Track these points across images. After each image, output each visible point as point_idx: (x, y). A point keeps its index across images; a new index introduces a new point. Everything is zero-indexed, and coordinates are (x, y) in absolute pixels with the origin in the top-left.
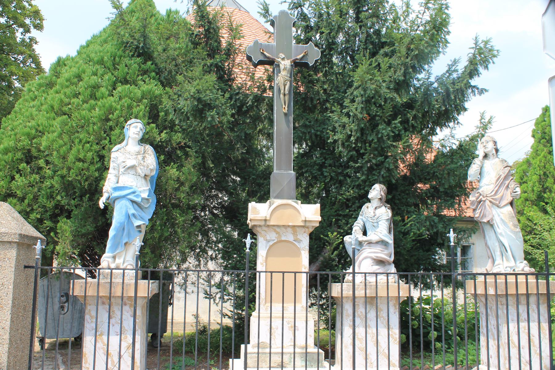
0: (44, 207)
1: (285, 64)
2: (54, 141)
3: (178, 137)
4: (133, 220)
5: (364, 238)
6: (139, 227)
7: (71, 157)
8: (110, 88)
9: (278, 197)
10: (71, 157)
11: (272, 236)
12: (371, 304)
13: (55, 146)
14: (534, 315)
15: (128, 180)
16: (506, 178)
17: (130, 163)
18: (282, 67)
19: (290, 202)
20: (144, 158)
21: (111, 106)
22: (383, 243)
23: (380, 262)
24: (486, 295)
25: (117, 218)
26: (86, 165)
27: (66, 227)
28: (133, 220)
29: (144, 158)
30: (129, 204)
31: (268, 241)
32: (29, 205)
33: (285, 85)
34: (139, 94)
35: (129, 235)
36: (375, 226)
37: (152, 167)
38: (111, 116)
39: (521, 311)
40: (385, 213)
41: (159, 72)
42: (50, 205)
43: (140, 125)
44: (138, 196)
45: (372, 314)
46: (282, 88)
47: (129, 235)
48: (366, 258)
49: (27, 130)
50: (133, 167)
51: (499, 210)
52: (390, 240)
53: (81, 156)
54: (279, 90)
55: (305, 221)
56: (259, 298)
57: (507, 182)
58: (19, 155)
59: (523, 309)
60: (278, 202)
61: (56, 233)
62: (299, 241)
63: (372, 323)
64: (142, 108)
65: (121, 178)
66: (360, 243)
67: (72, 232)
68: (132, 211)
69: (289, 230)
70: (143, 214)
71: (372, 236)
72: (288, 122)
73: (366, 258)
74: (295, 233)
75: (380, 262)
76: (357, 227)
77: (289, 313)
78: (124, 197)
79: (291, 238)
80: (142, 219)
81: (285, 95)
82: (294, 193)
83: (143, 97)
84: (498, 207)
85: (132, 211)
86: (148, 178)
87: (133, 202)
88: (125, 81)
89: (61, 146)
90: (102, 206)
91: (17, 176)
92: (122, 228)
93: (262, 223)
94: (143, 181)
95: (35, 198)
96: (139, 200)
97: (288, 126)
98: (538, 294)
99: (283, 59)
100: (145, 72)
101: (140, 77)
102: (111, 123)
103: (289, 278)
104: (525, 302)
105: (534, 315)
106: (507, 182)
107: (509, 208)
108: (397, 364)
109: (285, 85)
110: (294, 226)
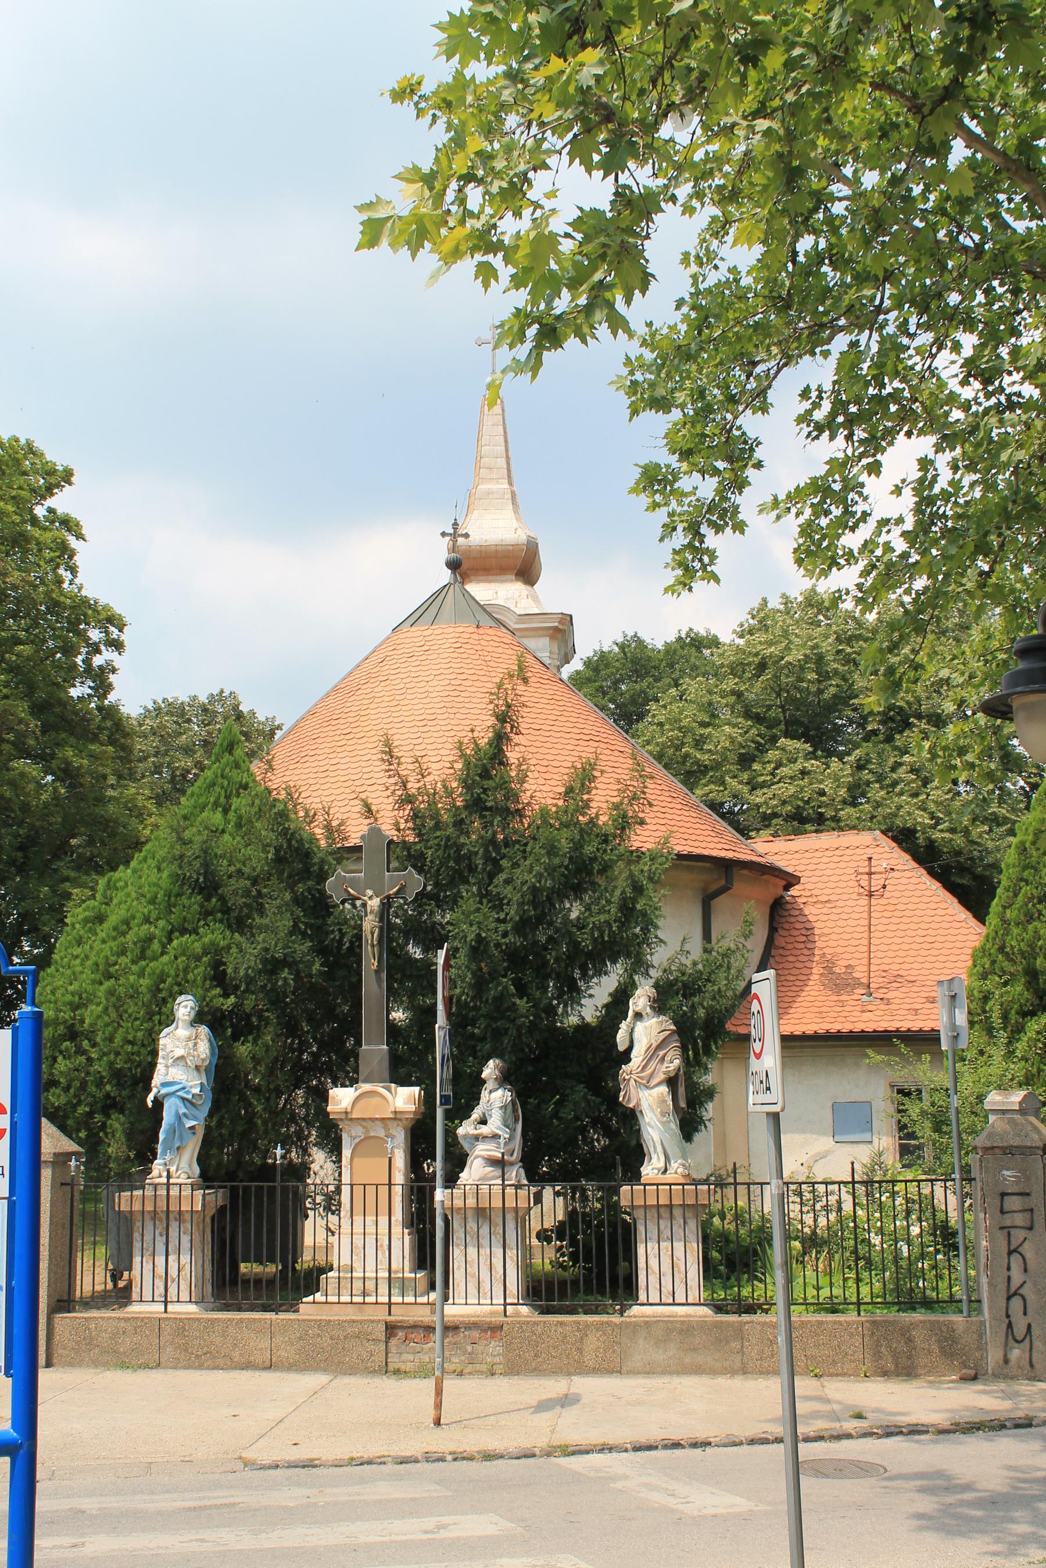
0: (93, 1096)
2: (99, 1017)
3: (249, 1002)
4: (185, 1120)
6: (192, 1128)
7: (118, 1040)
8: (164, 940)
10: (118, 1040)
11: (358, 1131)
12: (485, 1217)
14: (678, 1232)
15: (177, 1074)
16: (659, 1047)
20: (195, 1044)
21: (162, 971)
26: (136, 1048)
27: (117, 1125)
28: (185, 1120)
29: (195, 1044)
32: (75, 1096)
33: (372, 934)
34: (198, 947)
35: (181, 1138)
37: (203, 1056)
38: (162, 986)
39: (662, 1227)
41: (226, 910)
42: (100, 1095)
43: (191, 1004)
44: (188, 1092)
45: (485, 1230)
47: (181, 1138)
49: (68, 998)
50: (182, 1058)
51: (647, 1092)
53: (130, 1037)
55: (396, 1112)
57: (661, 1053)
58: (61, 1029)
59: (664, 1224)
60: (365, 1087)
61: (106, 1134)
63: (485, 1242)
64: (200, 971)
66: (477, 1138)
67: (124, 1131)
68: (183, 1110)
69: (378, 1123)
70: (196, 1112)
72: (379, 980)
73: (477, 1157)
74: (386, 1128)
76: (476, 1115)
78: (173, 1093)
79: (381, 1133)
80: (195, 1118)
81: (373, 946)
82: (386, 1074)
84: (647, 1088)
85: (183, 1110)
86: (202, 1069)
87: (183, 1099)
88: (183, 931)
89: (107, 1025)
90: (150, 1104)
91: (60, 1059)
92: (172, 1131)
93: (343, 1116)
94: (195, 1073)
95: (84, 1084)
96: (190, 1097)
97: (380, 986)
98: (645, 1206)
99: (370, 898)
100: (206, 914)
101: (202, 923)
102: (163, 994)
103: (371, 1191)
104: (668, 1215)
105: (678, 1232)
106: (661, 1053)
107: (664, 1089)
109: (372, 934)
110: (382, 1119)
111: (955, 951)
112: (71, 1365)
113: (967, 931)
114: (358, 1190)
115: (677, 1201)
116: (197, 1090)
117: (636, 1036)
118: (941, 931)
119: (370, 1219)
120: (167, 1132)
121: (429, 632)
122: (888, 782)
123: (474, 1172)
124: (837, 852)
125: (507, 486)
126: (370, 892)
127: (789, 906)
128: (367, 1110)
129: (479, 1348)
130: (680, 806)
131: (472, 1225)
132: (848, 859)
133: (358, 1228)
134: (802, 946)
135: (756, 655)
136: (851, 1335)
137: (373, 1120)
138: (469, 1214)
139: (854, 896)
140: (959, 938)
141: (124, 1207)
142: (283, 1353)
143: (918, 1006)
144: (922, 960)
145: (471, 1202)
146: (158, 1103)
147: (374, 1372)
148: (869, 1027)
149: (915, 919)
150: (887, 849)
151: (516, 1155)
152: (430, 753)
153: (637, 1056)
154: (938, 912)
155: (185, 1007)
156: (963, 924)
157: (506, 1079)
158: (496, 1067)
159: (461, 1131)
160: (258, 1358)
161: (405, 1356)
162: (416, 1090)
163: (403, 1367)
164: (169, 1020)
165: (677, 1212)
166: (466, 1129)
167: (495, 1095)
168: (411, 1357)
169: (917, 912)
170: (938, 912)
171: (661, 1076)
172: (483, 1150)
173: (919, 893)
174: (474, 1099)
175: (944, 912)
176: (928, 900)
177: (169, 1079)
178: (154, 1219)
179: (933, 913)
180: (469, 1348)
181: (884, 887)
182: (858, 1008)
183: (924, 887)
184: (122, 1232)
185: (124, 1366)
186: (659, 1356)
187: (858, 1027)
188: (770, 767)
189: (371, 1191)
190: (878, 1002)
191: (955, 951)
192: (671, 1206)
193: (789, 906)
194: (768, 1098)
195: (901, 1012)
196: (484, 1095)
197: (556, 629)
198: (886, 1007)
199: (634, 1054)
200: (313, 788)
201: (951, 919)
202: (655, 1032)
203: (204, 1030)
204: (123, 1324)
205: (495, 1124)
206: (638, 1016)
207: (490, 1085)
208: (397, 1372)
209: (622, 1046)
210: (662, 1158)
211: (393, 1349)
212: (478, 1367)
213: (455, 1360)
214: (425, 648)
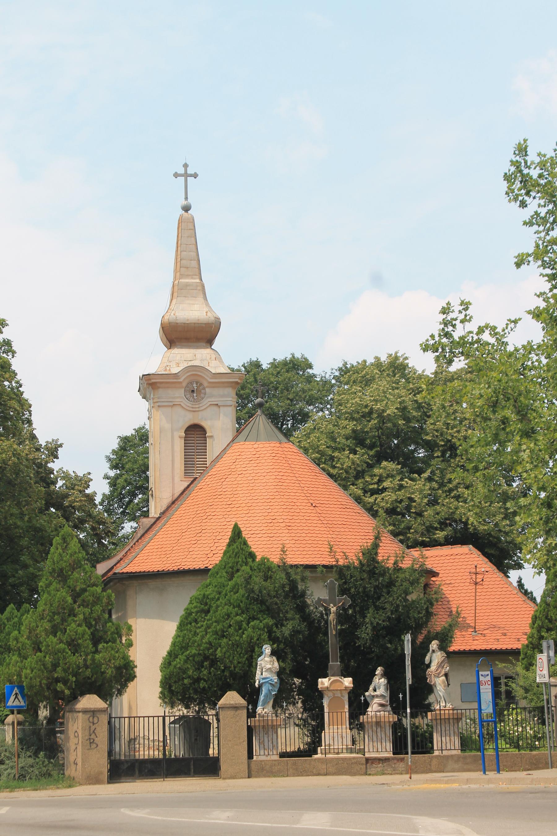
1: (333, 609)
5: (376, 693)
9: (333, 675)
11: (330, 694)
13: (226, 656)
16: (442, 662)
17: (269, 666)
18: (332, 611)
19: (338, 678)
22: (382, 696)
23: (382, 705)
24: (441, 719)
25: (264, 691)
30: (269, 685)
31: (329, 697)
36: (379, 688)
40: (383, 681)
44: (273, 681)
45: (379, 730)
46: (332, 622)
48: (375, 703)
50: (270, 669)
52: (387, 695)
54: (330, 621)
55: (346, 687)
56: (173, 461)
59: (447, 725)
60: (333, 678)
62: (343, 697)
64: (265, 636)
65: (264, 673)
66: (373, 696)
68: (271, 688)
71: (378, 693)
72: (336, 638)
73: (375, 703)
75: (382, 705)
76: (371, 688)
77: (340, 731)
79: (339, 695)
80: (275, 691)
82: (340, 674)
83: (264, 627)
85: (271, 688)
87: (271, 684)
98: (445, 719)
99: (332, 607)
103: (151, 719)
107: (444, 678)
108: (325, 714)
110: (340, 690)
111: (513, 609)
112: (256, 777)
113: (517, 599)
114: (331, 714)
115: (451, 717)
116: (276, 681)
117: (433, 658)
118: (505, 599)
119: (335, 727)
120: (264, 696)
121: (256, 446)
122: (446, 488)
124: (452, 557)
125: (198, 281)
126: (332, 605)
127: (431, 586)
128: (336, 687)
129: (397, 765)
130: (390, 542)
131: (374, 728)
132: (458, 561)
133: (331, 731)
134: (440, 607)
135: (366, 406)
136: (517, 758)
137: (337, 690)
138: (373, 724)
139: (468, 584)
140: (515, 602)
142: (330, 770)
144: (498, 614)
145: (374, 720)
146: (260, 686)
147: (362, 775)
148: (478, 648)
149: (493, 593)
150: (476, 555)
153: (433, 667)
154: (504, 589)
155: (267, 649)
156: (516, 596)
157: (385, 675)
158: (382, 670)
160: (322, 772)
161: (372, 769)
163: (371, 773)
165: (451, 721)
166: (370, 692)
167: (381, 681)
168: (374, 769)
169: (494, 589)
170: (504, 589)
171: (443, 673)
173: (494, 579)
175: (506, 589)
176: (498, 583)
177: (264, 676)
178: (272, 728)
179: (501, 590)
180: (393, 766)
181: (483, 580)
182: (471, 638)
183: (496, 576)
185: (275, 776)
186: (456, 766)
187: (473, 648)
188: (376, 479)
189: (151, 719)
190: (480, 635)
191: (513, 609)
192: (449, 719)
193: (431, 586)
194: (544, 679)
195: (491, 640)
198: (484, 638)
199: (433, 664)
200: (221, 534)
201: (510, 593)
202: (440, 657)
203: (274, 658)
204: (274, 762)
205: (381, 691)
206: (433, 651)
208: (370, 775)
209: (427, 662)
210: (444, 702)
211: (368, 767)
212: (396, 772)
213: (389, 770)
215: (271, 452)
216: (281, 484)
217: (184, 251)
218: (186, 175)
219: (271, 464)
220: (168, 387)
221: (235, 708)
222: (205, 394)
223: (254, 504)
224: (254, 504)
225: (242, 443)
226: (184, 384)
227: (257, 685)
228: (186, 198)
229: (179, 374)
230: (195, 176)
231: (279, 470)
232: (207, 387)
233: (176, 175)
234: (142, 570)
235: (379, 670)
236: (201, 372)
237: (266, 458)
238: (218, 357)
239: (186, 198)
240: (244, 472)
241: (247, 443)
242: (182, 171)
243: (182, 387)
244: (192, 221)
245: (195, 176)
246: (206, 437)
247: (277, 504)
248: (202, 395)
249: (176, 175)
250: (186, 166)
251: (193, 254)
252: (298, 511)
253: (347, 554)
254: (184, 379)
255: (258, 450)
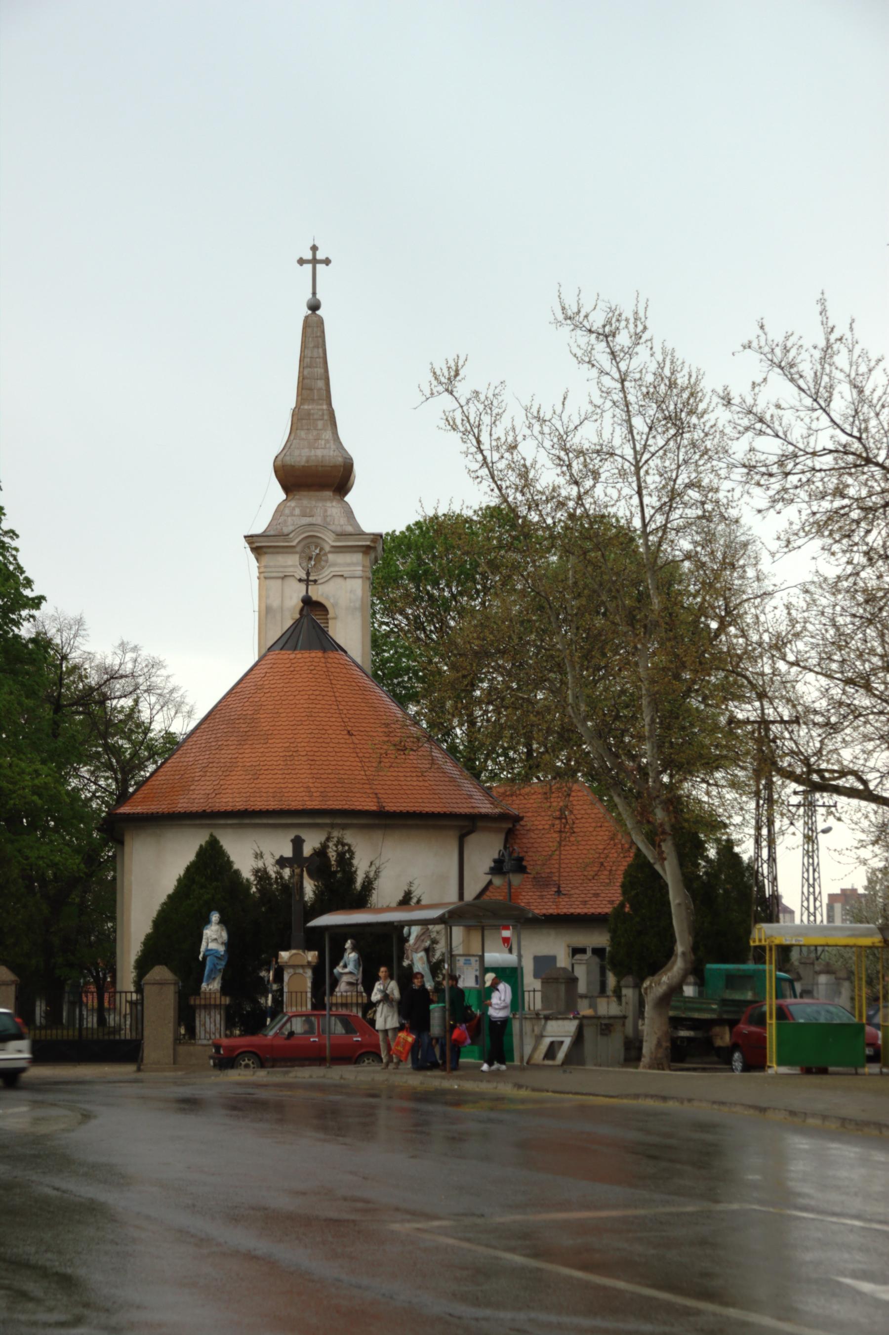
9: (295, 948)
15: (212, 946)
19: (300, 952)
60: (294, 951)
76: (341, 964)
92: (211, 971)
103: (299, 994)
123: (342, 987)
141: (192, 1002)
143: (587, 899)
151: (360, 981)
152: (300, 749)
153: (412, 940)
155: (215, 917)
157: (354, 949)
159: (335, 971)
162: (316, 953)
164: (207, 922)
166: (339, 969)
171: (422, 948)
172: (345, 979)
174: (341, 957)
184: (140, 1030)
189: (299, 994)
196: (346, 955)
197: (368, 547)
207: (349, 951)
214: (292, 669)
215: (309, 664)
216: (314, 706)
217: (307, 367)
218: (314, 261)
219: (306, 680)
220: (278, 553)
221: (161, 983)
222: (327, 561)
223: (275, 732)
224: (275, 732)
225: (277, 652)
226: (298, 549)
227: (200, 957)
228: (314, 293)
229: (291, 536)
230: (327, 262)
231: (315, 688)
232: (330, 552)
233: (301, 262)
234: (150, 811)
235: (348, 944)
236: (317, 532)
237: (302, 672)
238: (349, 513)
239: (314, 293)
240: (272, 690)
241: (283, 652)
242: (308, 255)
243: (296, 553)
244: (320, 322)
245: (327, 262)
246: (327, 619)
247: (303, 731)
248: (323, 563)
249: (301, 262)
250: (314, 249)
251: (321, 371)
252: (328, 740)
253: (380, 796)
254: (299, 542)
255: (293, 661)
